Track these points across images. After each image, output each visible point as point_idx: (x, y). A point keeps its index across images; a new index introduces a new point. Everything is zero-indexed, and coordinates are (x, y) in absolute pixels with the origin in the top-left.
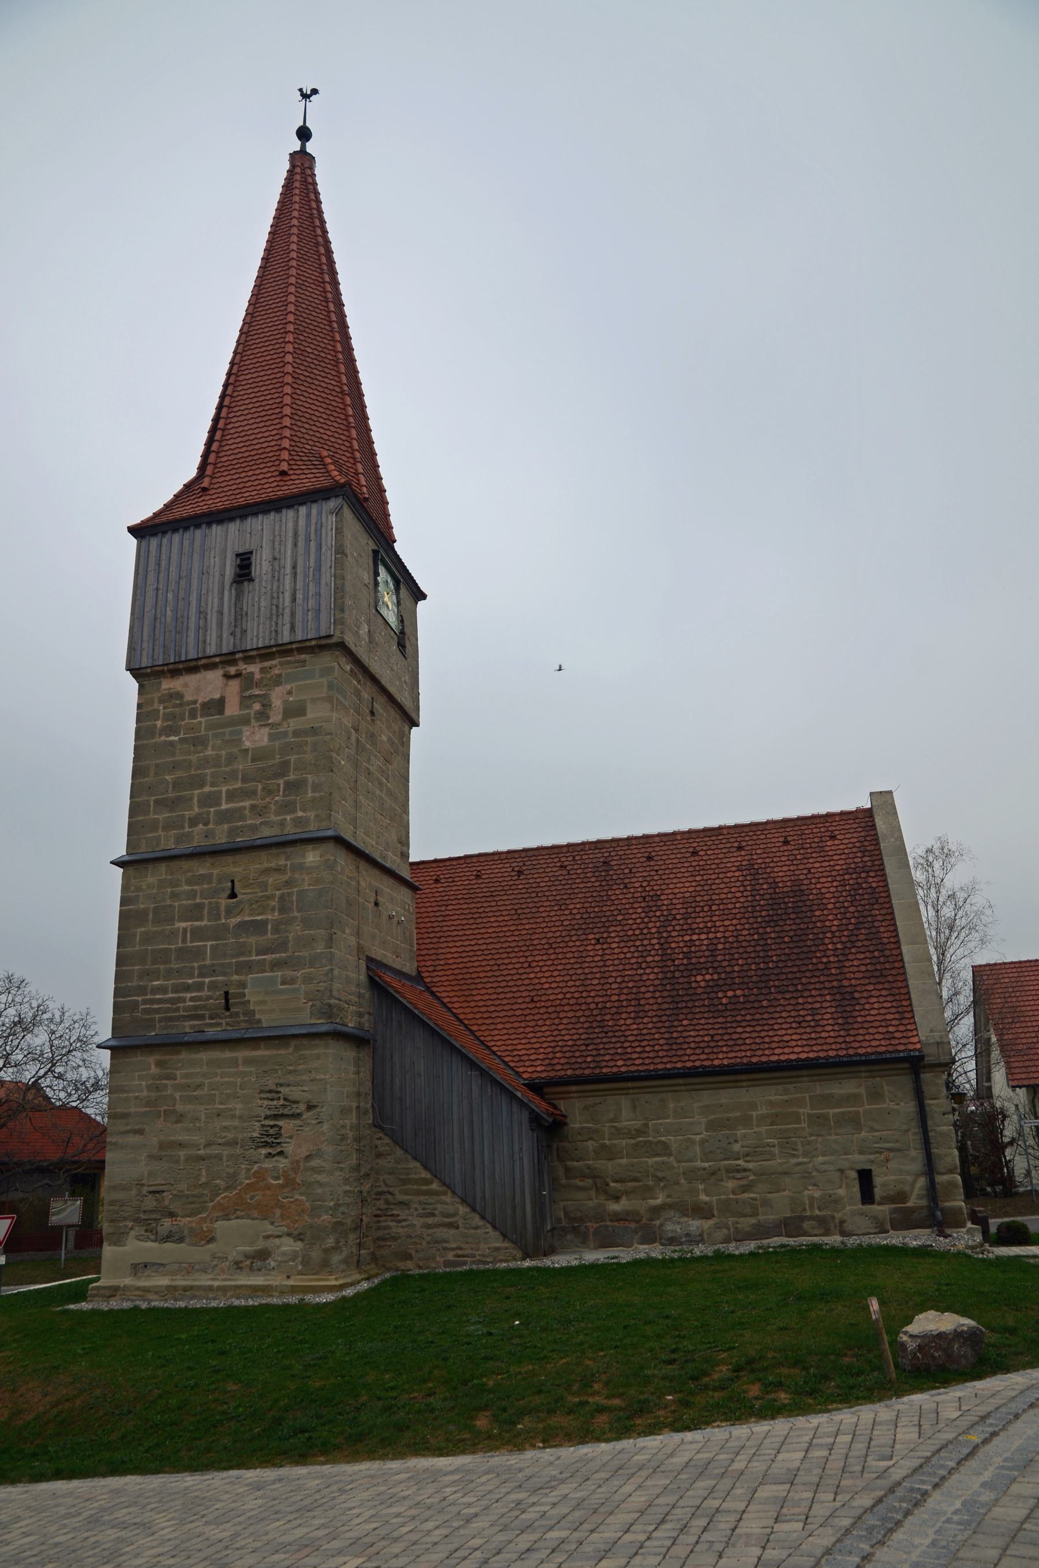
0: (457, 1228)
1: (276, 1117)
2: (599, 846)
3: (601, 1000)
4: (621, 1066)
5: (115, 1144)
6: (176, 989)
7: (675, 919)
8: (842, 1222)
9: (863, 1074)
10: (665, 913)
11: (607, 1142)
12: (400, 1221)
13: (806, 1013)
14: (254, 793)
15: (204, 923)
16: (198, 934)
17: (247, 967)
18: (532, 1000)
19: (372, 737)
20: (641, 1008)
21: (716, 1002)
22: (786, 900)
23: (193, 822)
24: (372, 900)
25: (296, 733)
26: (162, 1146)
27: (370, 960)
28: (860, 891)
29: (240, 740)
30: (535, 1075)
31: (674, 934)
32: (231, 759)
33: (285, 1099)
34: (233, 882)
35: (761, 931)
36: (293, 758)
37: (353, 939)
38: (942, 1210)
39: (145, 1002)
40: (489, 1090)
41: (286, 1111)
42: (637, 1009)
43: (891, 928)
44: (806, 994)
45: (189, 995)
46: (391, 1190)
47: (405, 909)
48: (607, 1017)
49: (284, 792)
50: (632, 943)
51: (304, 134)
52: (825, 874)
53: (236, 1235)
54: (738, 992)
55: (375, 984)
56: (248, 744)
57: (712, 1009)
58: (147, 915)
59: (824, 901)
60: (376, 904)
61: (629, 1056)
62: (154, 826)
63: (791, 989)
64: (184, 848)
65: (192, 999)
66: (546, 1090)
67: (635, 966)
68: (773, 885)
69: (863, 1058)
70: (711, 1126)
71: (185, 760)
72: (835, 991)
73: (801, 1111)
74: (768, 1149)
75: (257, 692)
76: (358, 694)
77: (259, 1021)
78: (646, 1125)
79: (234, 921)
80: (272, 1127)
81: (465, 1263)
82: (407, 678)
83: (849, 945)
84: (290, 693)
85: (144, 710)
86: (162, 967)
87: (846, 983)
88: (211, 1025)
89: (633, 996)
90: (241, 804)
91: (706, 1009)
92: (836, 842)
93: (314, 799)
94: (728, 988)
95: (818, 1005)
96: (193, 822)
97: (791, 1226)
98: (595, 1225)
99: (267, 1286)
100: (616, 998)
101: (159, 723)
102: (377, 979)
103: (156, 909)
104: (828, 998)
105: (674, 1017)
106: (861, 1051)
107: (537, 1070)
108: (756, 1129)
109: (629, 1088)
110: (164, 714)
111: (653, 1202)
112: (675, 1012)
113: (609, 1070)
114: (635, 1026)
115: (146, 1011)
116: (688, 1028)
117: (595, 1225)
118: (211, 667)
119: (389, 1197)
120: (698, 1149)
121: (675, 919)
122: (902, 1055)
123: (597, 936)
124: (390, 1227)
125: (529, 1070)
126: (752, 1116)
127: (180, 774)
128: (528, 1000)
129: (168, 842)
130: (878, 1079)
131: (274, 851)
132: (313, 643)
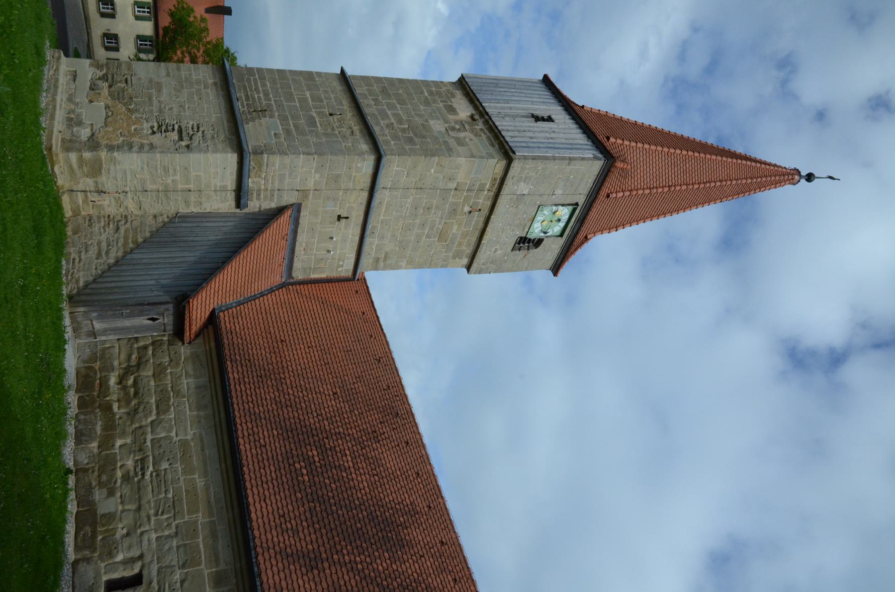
0: (97, 259)
8: (88, 560)
11: (169, 371)
12: (104, 228)
17: (283, 119)
36: (428, 140)
39: (255, 80)
45: (261, 95)
46: (129, 223)
51: (810, 177)
65: (259, 98)
66: (210, 327)
69: (254, 560)
70: (184, 444)
73: (200, 514)
74: (163, 489)
78: (184, 397)
79: (314, 115)
81: (68, 263)
97: (88, 517)
98: (97, 368)
106: (260, 558)
108: (182, 479)
111: (115, 407)
117: (97, 368)
118: (476, 107)
119: (123, 222)
120: (163, 435)
126: (194, 474)
128: (283, 338)
129: (358, 91)
130: (234, 581)
131: (365, 131)
132: (507, 147)
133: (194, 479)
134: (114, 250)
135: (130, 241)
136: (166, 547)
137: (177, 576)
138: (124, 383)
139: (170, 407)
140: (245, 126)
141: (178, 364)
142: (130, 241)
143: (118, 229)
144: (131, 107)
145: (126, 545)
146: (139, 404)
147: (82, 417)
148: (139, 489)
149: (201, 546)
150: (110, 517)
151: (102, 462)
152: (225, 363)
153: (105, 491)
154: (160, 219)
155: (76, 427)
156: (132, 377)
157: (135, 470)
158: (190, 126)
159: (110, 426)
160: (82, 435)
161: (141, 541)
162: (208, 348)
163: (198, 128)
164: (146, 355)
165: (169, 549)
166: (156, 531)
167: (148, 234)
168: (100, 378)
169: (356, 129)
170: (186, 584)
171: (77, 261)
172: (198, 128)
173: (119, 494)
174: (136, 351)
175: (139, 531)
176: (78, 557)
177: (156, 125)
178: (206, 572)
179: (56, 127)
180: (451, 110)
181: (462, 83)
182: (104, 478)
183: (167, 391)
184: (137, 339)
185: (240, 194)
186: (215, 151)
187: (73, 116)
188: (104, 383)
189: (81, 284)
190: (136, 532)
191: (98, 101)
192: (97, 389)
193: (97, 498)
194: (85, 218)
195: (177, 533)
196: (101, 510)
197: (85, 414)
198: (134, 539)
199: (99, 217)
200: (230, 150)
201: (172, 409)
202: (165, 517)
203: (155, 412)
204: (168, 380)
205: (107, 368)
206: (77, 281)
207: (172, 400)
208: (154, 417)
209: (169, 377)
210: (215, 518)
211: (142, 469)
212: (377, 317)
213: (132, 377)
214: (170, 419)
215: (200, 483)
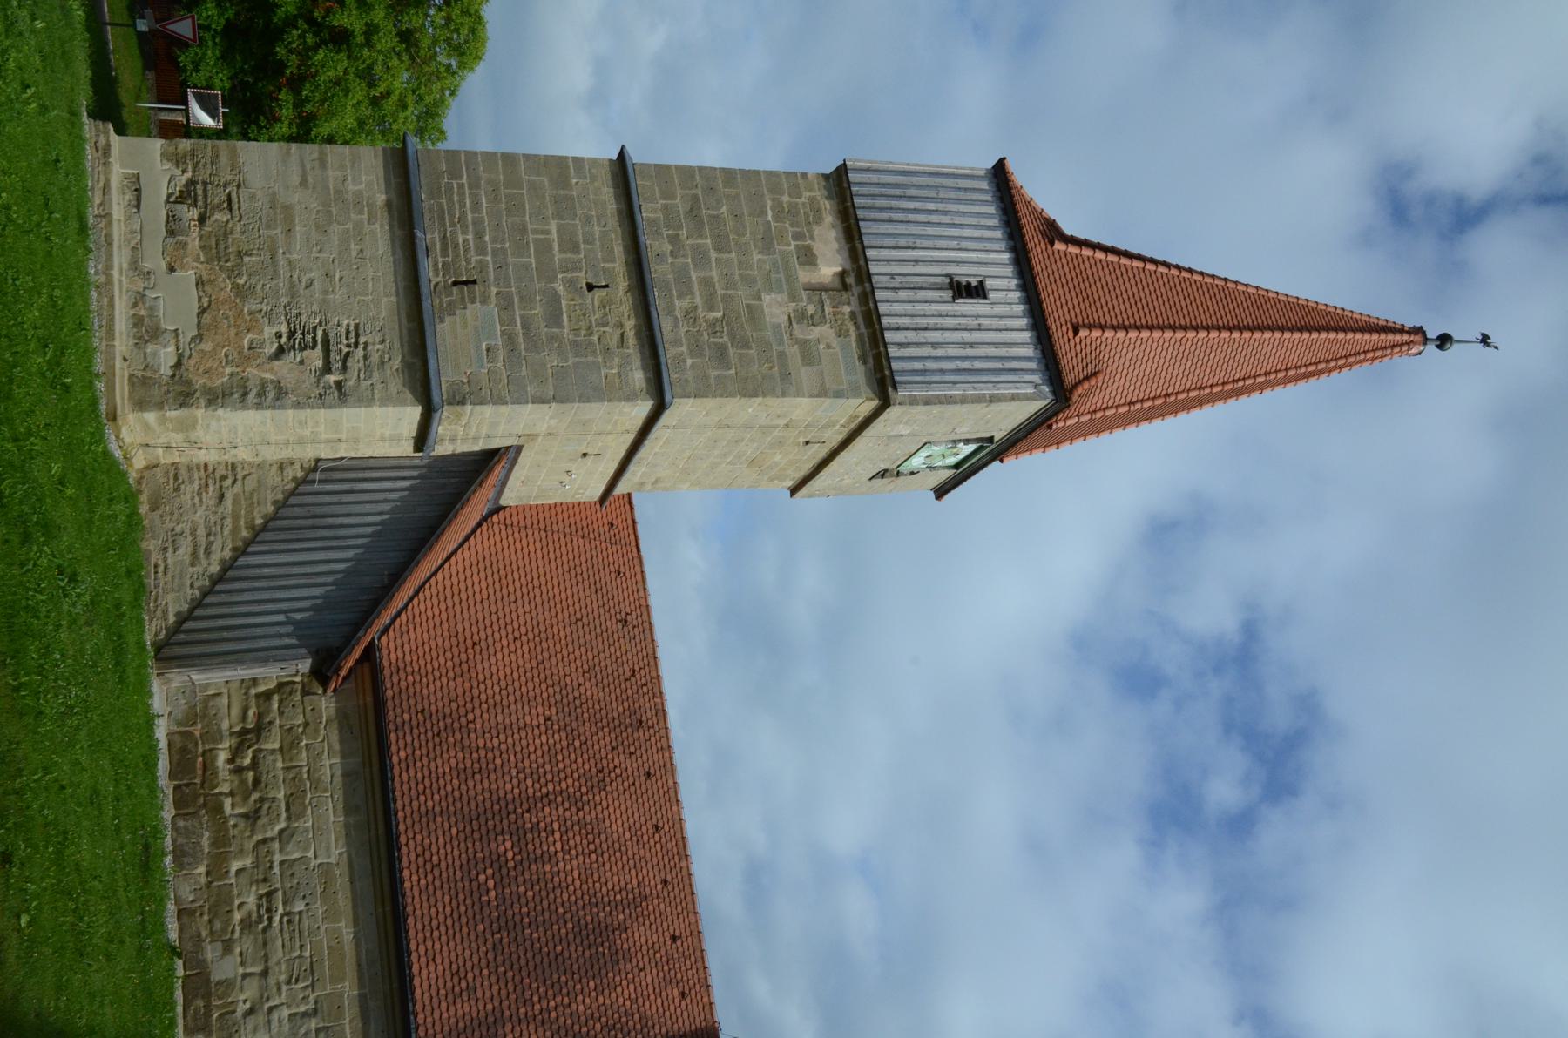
5: (288, 153)
15: (557, 256)
16: (544, 247)
17: (506, 304)
23: (674, 240)
33: (348, 354)
39: (461, 186)
41: (333, 355)
45: (470, 237)
46: (239, 483)
53: (177, 302)
56: (767, 298)
70: (325, 870)
78: (326, 791)
79: (561, 290)
96: (674, 240)
98: (197, 734)
111: (228, 802)
117: (197, 734)
120: (296, 855)
129: (648, 212)
134: (216, 547)
135: (242, 524)
136: (303, 1030)
138: (238, 761)
139: (305, 808)
140: (439, 327)
141: (317, 731)
142: (242, 524)
143: (221, 497)
144: (241, 282)
145: (250, 1027)
146: (262, 800)
147: (181, 823)
148: (265, 944)
149: (348, 1031)
150: (228, 985)
152: (388, 737)
154: (290, 473)
155: (174, 841)
156: (250, 752)
161: (269, 1022)
163: (357, 336)
164: (269, 711)
166: (289, 1006)
167: (270, 509)
169: (630, 324)
171: (161, 569)
172: (357, 336)
174: (253, 702)
175: (266, 1006)
177: (284, 329)
179: (118, 348)
180: (808, 257)
181: (839, 181)
182: (218, 925)
183: (301, 780)
184: (255, 682)
185: (422, 439)
186: (385, 402)
187: (142, 313)
188: (209, 755)
189: (172, 619)
191: (182, 268)
192: (200, 772)
193: (209, 956)
194: (167, 473)
196: (216, 976)
198: (261, 1018)
199: (190, 469)
200: (409, 396)
201: (309, 811)
202: (301, 985)
203: (284, 815)
205: (213, 736)
206: (165, 613)
208: (283, 825)
211: (269, 910)
212: (634, 522)
213: (250, 752)
214: (306, 830)
215: (347, 933)
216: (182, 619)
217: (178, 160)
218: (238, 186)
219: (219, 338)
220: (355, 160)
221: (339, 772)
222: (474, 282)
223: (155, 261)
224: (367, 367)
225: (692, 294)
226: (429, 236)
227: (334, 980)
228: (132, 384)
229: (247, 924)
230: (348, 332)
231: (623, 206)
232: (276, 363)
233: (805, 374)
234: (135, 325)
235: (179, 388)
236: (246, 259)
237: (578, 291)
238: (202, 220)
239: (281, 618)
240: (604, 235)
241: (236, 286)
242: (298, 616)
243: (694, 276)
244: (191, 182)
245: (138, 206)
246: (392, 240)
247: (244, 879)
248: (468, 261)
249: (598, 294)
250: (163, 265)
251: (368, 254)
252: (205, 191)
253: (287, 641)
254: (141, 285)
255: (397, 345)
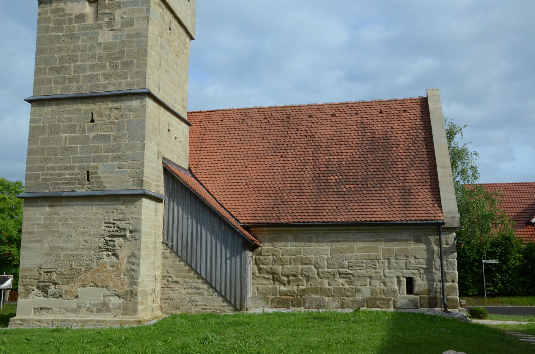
0: (203, 295)
1: (112, 236)
2: (285, 108)
3: (282, 186)
4: (290, 219)
5: (26, 247)
6: (60, 169)
7: (321, 147)
8: (395, 302)
9: (412, 230)
10: (317, 144)
11: (281, 256)
13: (385, 198)
14: (105, 67)
15: (77, 134)
16: (73, 140)
17: (99, 159)
18: (247, 184)
19: (169, 42)
20: (302, 191)
21: (340, 190)
22: (379, 141)
23: (71, 81)
24: (167, 128)
25: (128, 36)
26: (51, 249)
27: (164, 158)
28: (418, 139)
29: (97, 38)
30: (246, 221)
31: (321, 155)
32: (92, 48)
33: (118, 227)
34: (92, 114)
35: (365, 156)
36: (126, 49)
37: (155, 147)
38: (447, 299)
39: (43, 174)
40: (223, 228)
41: (118, 233)
42: (300, 191)
43: (432, 159)
44: (386, 189)
45: (67, 172)
46: (170, 275)
47: (183, 135)
48: (285, 195)
49: (121, 67)
50: (299, 159)
52: (400, 129)
53: (91, 295)
54: (352, 186)
55: (167, 172)
56: (101, 40)
57: (338, 193)
58: (45, 129)
59: (399, 143)
60: (169, 130)
61: (294, 214)
62: (49, 81)
63: (379, 185)
64: (66, 94)
67: (300, 170)
68: (373, 133)
70: (333, 252)
71: (66, 47)
72: (401, 188)
73: (379, 246)
75: (107, 11)
76: (162, 17)
77: (105, 187)
78: (301, 249)
79: (93, 134)
80: (110, 241)
82: (189, 12)
83: (410, 165)
84: (125, 13)
85: (42, 17)
86: (53, 157)
87: (407, 184)
88: (79, 188)
89: (298, 185)
90: (97, 72)
91: (335, 193)
92: (407, 114)
93: (136, 72)
94: (346, 183)
95: (391, 195)
96: (71, 81)
98: (272, 297)
99: (104, 320)
100: (290, 185)
101: (51, 25)
102: (168, 169)
103: (49, 126)
104: (397, 191)
105: (319, 196)
107: (247, 219)
109: (293, 231)
110: (54, 20)
111: (301, 287)
112: (319, 194)
113: (284, 221)
114: (298, 200)
115: (44, 180)
116: (325, 202)
117: (272, 297)
120: (326, 262)
121: (321, 147)
122: (433, 222)
123: (281, 154)
124: (169, 293)
125: (243, 218)
127: (63, 54)
131: (115, 98)
133: (357, 248)
134: (197, 285)
135: (188, 275)
136: (395, 265)
137: (413, 260)
139: (307, 258)
141: (276, 251)
142: (188, 275)
147: (307, 305)
148: (359, 277)
149: (398, 247)
150: (373, 291)
151: (339, 295)
153: (357, 294)
154: (168, 254)
155: (314, 308)
157: (346, 278)
158: (107, 229)
159: (316, 291)
160: (319, 305)
162: (266, 232)
165: (396, 263)
166: (385, 269)
167: (182, 263)
168: (281, 295)
169: (110, 105)
170: (417, 257)
171: (204, 307)
172: (110, 223)
173: (360, 287)
174: (262, 275)
175: (383, 277)
176: (393, 307)
177: (105, 253)
178: (413, 246)
179: (111, 319)
180: (81, 17)
182: (349, 294)
183: (295, 258)
184: (253, 274)
185: (158, 200)
190: (383, 279)
192: (288, 297)
195: (388, 259)
196: (369, 295)
197: (304, 303)
198: (387, 280)
199: (163, 294)
200: (138, 203)
201: (309, 256)
202: (377, 264)
203: (309, 266)
204: (287, 257)
206: (222, 306)
207: (302, 256)
208: (313, 267)
209: (285, 256)
210: (383, 239)
212: (200, 112)
215: (360, 245)
216: (225, 300)
217: (28, 292)
218: (41, 268)
219: (108, 279)
220: (29, 219)
221: (294, 243)
222: (88, 172)
223: (74, 303)
224: (124, 220)
225: (97, 75)
226: (66, 190)
227: (378, 251)
228: (126, 314)
229: (350, 283)
230: (108, 227)
231: (54, 103)
232: (120, 257)
233: (138, 26)
234: (101, 312)
235: (129, 296)
236: (73, 267)
237: (94, 126)
238: (55, 284)
239: (228, 262)
240: (68, 113)
241: (86, 271)
242: (228, 255)
243: (89, 73)
244: (38, 287)
245: (48, 309)
246: (67, 206)
247: (332, 283)
248: (78, 174)
249: (95, 118)
250: (75, 300)
251: (73, 216)
252: (42, 282)
253: (238, 260)
254: (83, 309)
255: (115, 207)
